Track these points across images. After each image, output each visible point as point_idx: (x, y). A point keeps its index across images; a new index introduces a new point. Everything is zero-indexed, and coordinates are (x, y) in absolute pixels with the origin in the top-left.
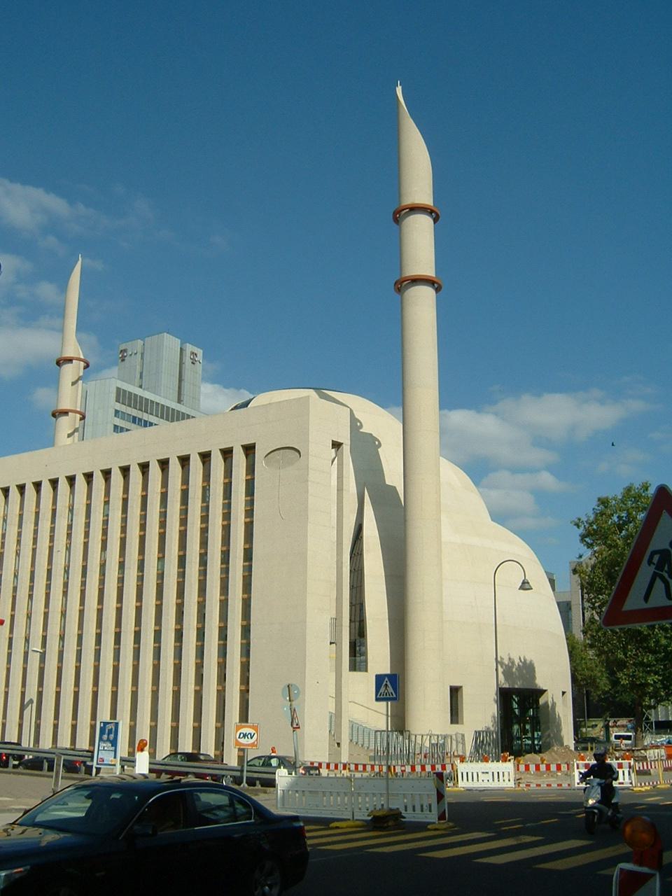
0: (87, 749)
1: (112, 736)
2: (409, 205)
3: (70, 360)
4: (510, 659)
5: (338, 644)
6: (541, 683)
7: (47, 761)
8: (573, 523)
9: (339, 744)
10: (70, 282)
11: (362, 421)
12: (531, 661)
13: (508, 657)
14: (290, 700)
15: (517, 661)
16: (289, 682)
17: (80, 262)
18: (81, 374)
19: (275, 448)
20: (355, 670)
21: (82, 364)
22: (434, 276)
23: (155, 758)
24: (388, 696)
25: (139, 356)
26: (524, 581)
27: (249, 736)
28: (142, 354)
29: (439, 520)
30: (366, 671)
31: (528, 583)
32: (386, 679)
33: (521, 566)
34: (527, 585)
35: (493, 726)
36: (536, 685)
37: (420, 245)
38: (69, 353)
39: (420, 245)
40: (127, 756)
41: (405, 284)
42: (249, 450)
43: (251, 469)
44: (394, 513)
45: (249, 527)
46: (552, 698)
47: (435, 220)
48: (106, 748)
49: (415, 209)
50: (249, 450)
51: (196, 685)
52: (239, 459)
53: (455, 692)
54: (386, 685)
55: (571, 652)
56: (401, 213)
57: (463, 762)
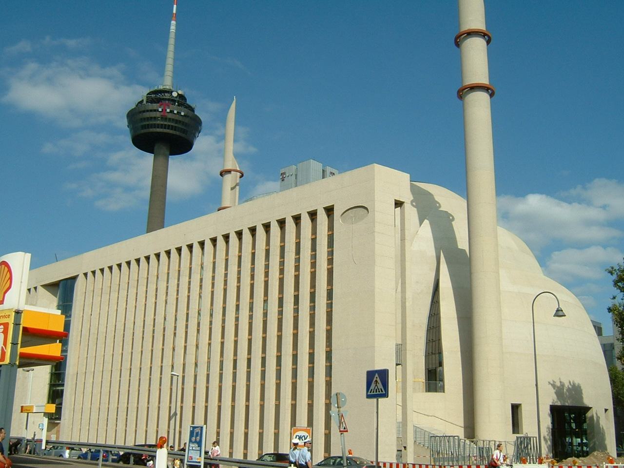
0: (273, 452)
1: (198, 438)
2: (466, 31)
3: (229, 172)
4: (561, 382)
5: (403, 365)
6: (587, 402)
7: (133, 456)
8: (608, 271)
9: (405, 447)
10: (228, 116)
11: (439, 202)
12: (579, 384)
13: (559, 381)
14: (338, 408)
15: (567, 384)
16: (339, 392)
17: (234, 101)
18: (238, 182)
19: (349, 208)
20: (429, 391)
21: (239, 174)
22: (488, 83)
23: (247, 459)
24: (378, 393)
25: (294, 177)
26: (558, 308)
27: (303, 438)
28: (296, 175)
29: (498, 273)
30: (444, 392)
31: (562, 311)
32: (377, 375)
33: (553, 294)
34: (561, 312)
35: (548, 435)
36: (583, 403)
37: (476, 62)
38: (229, 167)
39: (476, 62)
40: (228, 457)
41: (464, 91)
42: (329, 210)
43: (331, 227)
44: (461, 265)
45: (330, 272)
46: (597, 414)
47: (488, 42)
48: (194, 448)
49: (471, 34)
50: (329, 210)
51: (292, 400)
52: (322, 217)
53: (515, 408)
54: (376, 381)
55: (614, 380)
56: (459, 39)
57: (541, 463)
